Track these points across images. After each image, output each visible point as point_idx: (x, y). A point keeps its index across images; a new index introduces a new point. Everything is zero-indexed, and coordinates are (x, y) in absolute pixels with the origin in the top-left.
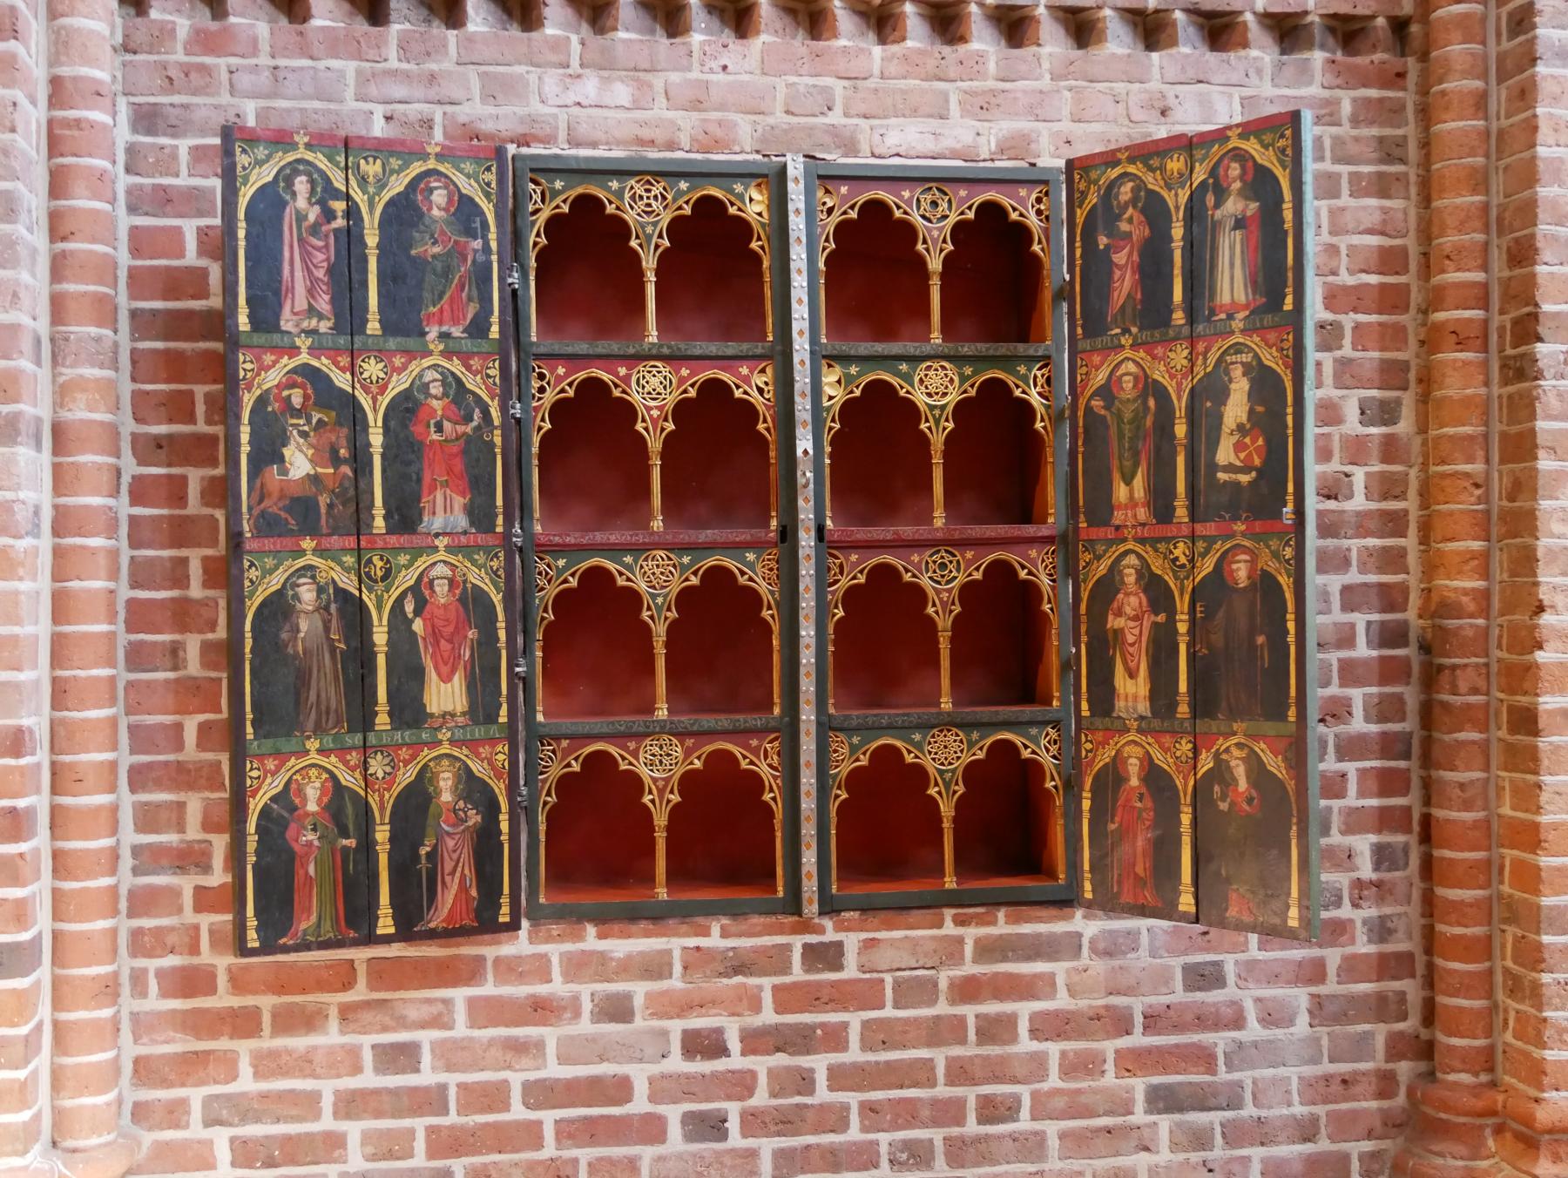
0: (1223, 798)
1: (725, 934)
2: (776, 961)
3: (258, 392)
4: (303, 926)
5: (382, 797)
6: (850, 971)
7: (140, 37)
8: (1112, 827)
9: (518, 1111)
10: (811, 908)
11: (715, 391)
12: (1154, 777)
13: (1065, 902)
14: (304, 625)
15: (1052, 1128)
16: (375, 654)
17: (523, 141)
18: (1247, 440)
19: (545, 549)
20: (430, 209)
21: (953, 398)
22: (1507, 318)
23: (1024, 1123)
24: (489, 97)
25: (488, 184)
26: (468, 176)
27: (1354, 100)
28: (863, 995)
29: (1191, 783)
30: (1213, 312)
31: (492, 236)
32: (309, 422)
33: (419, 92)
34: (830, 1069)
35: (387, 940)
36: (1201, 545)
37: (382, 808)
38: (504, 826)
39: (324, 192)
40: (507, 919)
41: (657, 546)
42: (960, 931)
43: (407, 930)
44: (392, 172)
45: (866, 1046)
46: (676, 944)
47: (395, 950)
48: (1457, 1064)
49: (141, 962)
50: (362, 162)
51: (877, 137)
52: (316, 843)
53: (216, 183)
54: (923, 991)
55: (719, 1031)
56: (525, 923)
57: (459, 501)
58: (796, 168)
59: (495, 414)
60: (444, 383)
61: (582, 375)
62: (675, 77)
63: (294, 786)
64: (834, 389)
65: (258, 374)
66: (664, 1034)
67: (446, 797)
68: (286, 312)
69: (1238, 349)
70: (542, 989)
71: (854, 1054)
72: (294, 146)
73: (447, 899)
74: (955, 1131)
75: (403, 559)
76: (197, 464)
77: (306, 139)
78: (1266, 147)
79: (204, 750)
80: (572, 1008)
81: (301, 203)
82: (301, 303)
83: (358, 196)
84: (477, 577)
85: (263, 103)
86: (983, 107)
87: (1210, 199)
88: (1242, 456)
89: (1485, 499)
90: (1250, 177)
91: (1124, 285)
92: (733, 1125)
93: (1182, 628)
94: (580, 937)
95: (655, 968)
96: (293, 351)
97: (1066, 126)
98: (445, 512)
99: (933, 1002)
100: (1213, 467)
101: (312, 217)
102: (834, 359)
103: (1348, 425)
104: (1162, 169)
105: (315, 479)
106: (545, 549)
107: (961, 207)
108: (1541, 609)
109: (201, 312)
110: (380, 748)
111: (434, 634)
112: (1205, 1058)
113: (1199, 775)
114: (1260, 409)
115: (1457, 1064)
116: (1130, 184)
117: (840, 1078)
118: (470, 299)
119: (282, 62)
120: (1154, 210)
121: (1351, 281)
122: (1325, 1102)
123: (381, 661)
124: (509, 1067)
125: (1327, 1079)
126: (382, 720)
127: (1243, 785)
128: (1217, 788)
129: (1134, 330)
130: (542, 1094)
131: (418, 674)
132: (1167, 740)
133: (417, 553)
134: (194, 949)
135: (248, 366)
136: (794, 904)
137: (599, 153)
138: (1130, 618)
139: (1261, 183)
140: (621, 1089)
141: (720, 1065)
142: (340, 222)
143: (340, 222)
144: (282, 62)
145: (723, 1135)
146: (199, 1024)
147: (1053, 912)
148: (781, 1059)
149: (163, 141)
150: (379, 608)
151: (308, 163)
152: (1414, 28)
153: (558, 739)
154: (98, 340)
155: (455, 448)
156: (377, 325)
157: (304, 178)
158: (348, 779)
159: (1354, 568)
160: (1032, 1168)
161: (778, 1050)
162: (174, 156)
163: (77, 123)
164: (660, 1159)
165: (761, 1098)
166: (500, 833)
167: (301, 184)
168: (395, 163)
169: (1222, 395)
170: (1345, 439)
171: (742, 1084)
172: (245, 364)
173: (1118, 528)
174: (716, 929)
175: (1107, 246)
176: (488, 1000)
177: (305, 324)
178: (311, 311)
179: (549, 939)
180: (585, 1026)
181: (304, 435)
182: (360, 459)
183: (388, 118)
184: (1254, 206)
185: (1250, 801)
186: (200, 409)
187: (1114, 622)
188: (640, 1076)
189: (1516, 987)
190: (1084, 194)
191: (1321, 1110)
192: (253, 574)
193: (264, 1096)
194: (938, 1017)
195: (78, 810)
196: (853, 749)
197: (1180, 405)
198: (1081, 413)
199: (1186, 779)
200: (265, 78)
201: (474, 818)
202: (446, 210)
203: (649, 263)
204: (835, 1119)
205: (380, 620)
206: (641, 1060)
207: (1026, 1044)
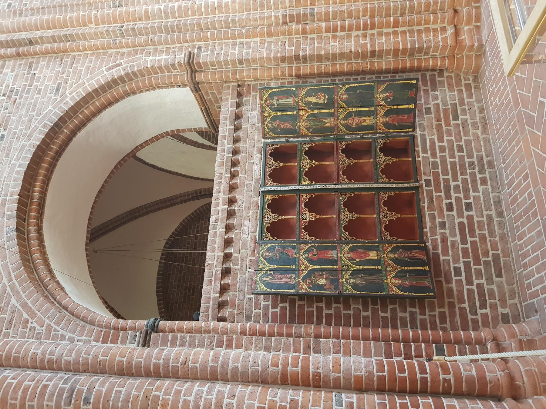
2: (430, 193)
6: (431, 178)
7: (231, 319)
9: (468, 246)
10: (417, 185)
11: (306, 205)
12: (386, 114)
13: (413, 137)
14: (359, 282)
15: (463, 138)
19: (340, 239)
21: (308, 161)
22: (295, 62)
23: (463, 143)
24: (246, 248)
28: (436, 176)
30: (294, 105)
33: (245, 262)
34: (453, 182)
36: (339, 106)
41: (339, 216)
45: (448, 174)
46: (427, 213)
48: (444, 63)
55: (446, 204)
57: (330, 252)
58: (263, 189)
61: (303, 231)
62: (244, 212)
64: (307, 182)
66: (448, 215)
67: (396, 256)
68: (291, 283)
70: (439, 240)
71: (450, 177)
73: (419, 256)
74: (466, 157)
75: (343, 262)
81: (268, 279)
82: (289, 280)
83: (267, 269)
84: (347, 249)
85: (246, 294)
86: (251, 156)
89: (329, 65)
91: (288, 125)
92: (468, 201)
93: (356, 109)
94: (427, 232)
95: (433, 217)
96: (299, 282)
97: (256, 142)
98: (333, 254)
100: (324, 104)
102: (300, 181)
104: (266, 117)
105: (326, 279)
106: (340, 239)
107: (271, 160)
108: (351, 51)
110: (386, 268)
111: (359, 257)
112: (446, 111)
115: (444, 63)
117: (455, 179)
119: (238, 289)
120: (274, 118)
122: (454, 88)
123: (366, 267)
124: (458, 247)
125: (449, 88)
126: (379, 267)
127: (387, 94)
130: (464, 241)
132: (378, 112)
133: (342, 260)
136: (417, 188)
138: (353, 122)
140: (461, 224)
141: (454, 204)
143: (272, 272)
144: (238, 289)
145: (470, 203)
146: (452, 314)
147: (415, 139)
148: (452, 191)
149: (253, 315)
150: (354, 267)
152: (240, 83)
153: (381, 236)
154: (296, 327)
155: (319, 252)
158: (393, 274)
160: (473, 142)
161: (450, 192)
162: (256, 313)
163: (250, 329)
164: (477, 216)
165: (461, 195)
169: (310, 103)
171: (458, 199)
172: (302, 291)
174: (423, 205)
178: (290, 278)
180: (447, 231)
181: (317, 280)
182: (322, 270)
183: (250, 268)
184: (275, 97)
185: (391, 92)
186: (311, 309)
187: (354, 125)
188: (457, 220)
189: (427, 53)
190: (270, 135)
191: (456, 89)
192: (347, 291)
193: (469, 301)
195: (403, 336)
196: (382, 178)
197: (312, 112)
200: (241, 293)
203: (280, 217)
204: (465, 181)
206: (454, 220)
207: (445, 143)
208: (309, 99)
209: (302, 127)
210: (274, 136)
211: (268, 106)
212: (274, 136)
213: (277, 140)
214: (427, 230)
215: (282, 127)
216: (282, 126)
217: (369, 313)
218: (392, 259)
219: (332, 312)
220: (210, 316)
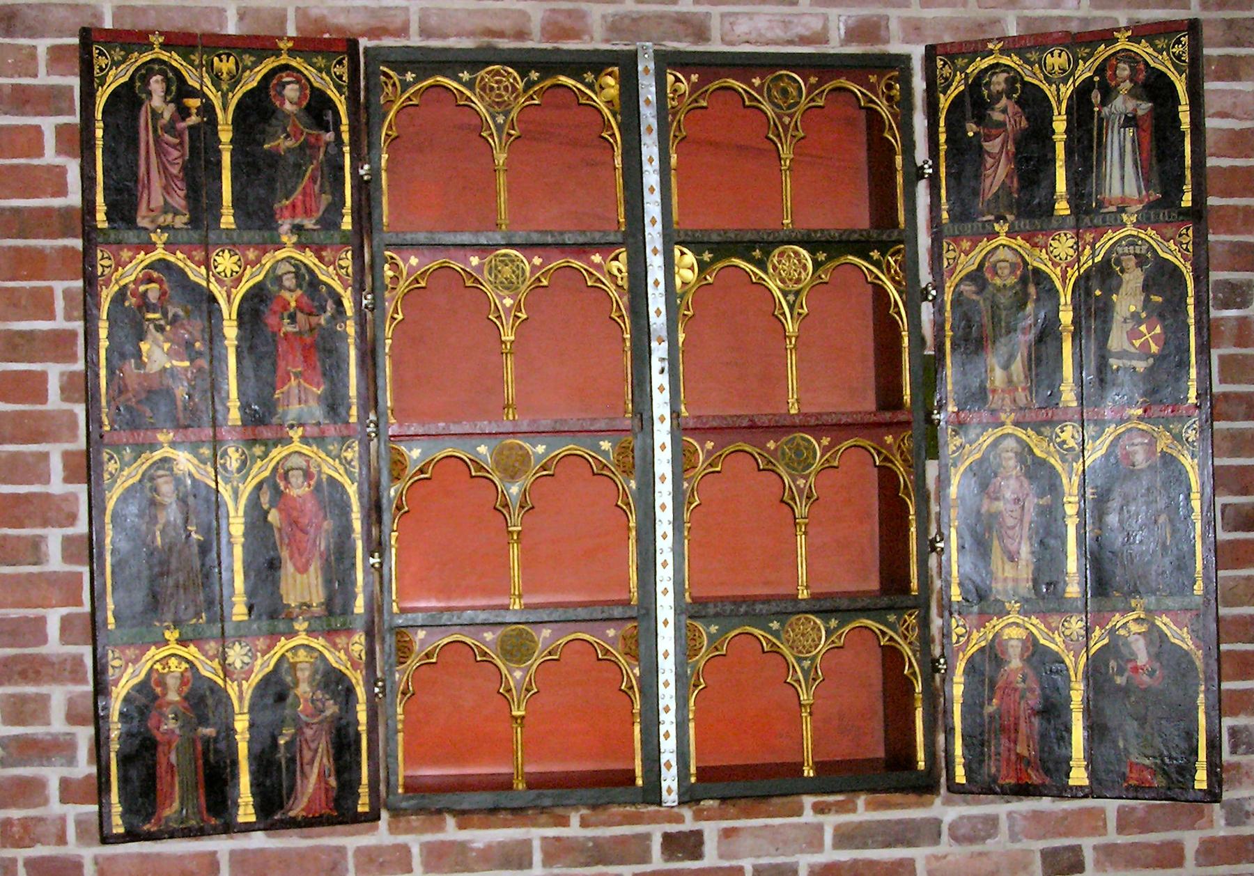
1: (584, 824)
3: (116, 288)
5: (240, 686)
17: (373, 33)
18: (1143, 328)
20: (283, 103)
25: (340, 77)
26: (320, 70)
29: (1083, 660)
30: (1100, 204)
31: (345, 128)
32: (165, 314)
35: (248, 828)
37: (241, 698)
38: (362, 717)
39: (180, 91)
40: (367, 809)
42: (821, 818)
44: (245, 69)
46: (536, 834)
47: (258, 840)
50: (216, 59)
51: (727, 26)
52: (177, 731)
53: (75, 82)
56: (384, 815)
59: (348, 304)
60: (297, 275)
63: (155, 676)
65: (116, 270)
72: (150, 47)
76: (56, 360)
77: (161, 40)
79: (67, 643)
81: (157, 102)
82: (158, 199)
84: (331, 469)
87: (1096, 97)
88: (1137, 343)
94: (440, 828)
96: (149, 247)
101: (167, 116)
104: (1042, 64)
109: (59, 209)
113: (1093, 651)
116: (1003, 76)
118: (322, 191)
120: (1034, 103)
127: (1142, 659)
128: (1112, 663)
129: (1010, 217)
131: (274, 565)
134: (62, 840)
135: (106, 262)
137: (452, 43)
139: (1156, 88)
142: (194, 119)
147: (912, 797)
151: (164, 62)
156: (231, 219)
157: (159, 77)
167: (156, 84)
168: (248, 59)
172: (103, 261)
174: (575, 819)
177: (161, 220)
179: (409, 830)
181: (160, 329)
185: (1151, 674)
186: (59, 305)
190: (948, 83)
199: (1076, 656)
201: (332, 709)
202: (298, 104)
205: (237, 510)
209: (985, 246)
210: (944, 102)
211: (1100, 70)
212: (944, 102)
213: (920, 123)
214: (451, 831)
215: (987, 146)
216: (993, 146)
217: (55, 562)
219: (54, 400)
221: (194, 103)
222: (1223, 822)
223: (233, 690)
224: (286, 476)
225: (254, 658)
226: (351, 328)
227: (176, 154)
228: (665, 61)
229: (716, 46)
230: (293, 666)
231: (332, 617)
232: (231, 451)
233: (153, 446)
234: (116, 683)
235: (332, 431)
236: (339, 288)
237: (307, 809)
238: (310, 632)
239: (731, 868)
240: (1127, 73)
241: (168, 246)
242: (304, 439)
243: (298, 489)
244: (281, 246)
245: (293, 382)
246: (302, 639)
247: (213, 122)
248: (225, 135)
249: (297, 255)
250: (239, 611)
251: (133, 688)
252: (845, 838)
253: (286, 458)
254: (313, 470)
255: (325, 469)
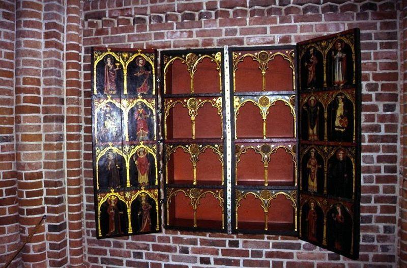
0: (335, 217)
1: (210, 236)
2: (222, 244)
4: (112, 231)
6: (241, 247)
8: (307, 220)
16: (126, 169)
26: (148, 57)
27: (381, 23)
31: (153, 70)
37: (129, 205)
42: (269, 240)
43: (136, 232)
46: (199, 238)
49: (88, 229)
51: (248, 40)
54: (259, 254)
55: (209, 258)
59: (154, 113)
60: (142, 105)
69: (341, 94)
70: (168, 244)
72: (107, 51)
78: (347, 38)
80: (175, 249)
84: (150, 151)
87: (333, 53)
90: (343, 46)
91: (311, 76)
94: (177, 234)
95: (194, 242)
99: (261, 257)
101: (111, 67)
103: (380, 111)
104: (321, 45)
114: (346, 111)
116: (312, 49)
120: (318, 55)
121: (381, 72)
131: (137, 174)
136: (226, 231)
139: (346, 49)
147: (293, 238)
157: (109, 58)
159: (381, 151)
166: (156, 210)
167: (109, 60)
169: (336, 107)
170: (379, 115)
173: (310, 141)
174: (208, 235)
175: (307, 66)
176: (130, 261)
180: (178, 253)
181: (110, 118)
185: (341, 219)
190: (301, 52)
194: (262, 261)
198: (301, 110)
201: (150, 207)
208: (341, 105)
214: (179, 235)
215: (309, 68)
216: (310, 69)
218: (139, 198)
220: (174, 13)
221: (118, 64)
222: (381, 251)
223: (127, 203)
224: (139, 153)
225: (132, 196)
226: (155, 118)
227: (113, 76)
228: (231, 50)
229: (245, 46)
230: (141, 197)
231: (151, 186)
232: (126, 147)
233: (108, 146)
234: (99, 202)
235: (151, 142)
236: (152, 108)
237: (145, 230)
238: (145, 189)
239: (246, 250)
240: (340, 46)
241: (111, 98)
242: (143, 144)
243: (142, 156)
244: (138, 98)
245: (141, 131)
246: (143, 191)
247: (123, 69)
248: (125, 72)
249: (142, 100)
250: (128, 185)
251: (104, 203)
252: (275, 246)
253: (139, 149)
254: (146, 151)
255: (149, 151)
